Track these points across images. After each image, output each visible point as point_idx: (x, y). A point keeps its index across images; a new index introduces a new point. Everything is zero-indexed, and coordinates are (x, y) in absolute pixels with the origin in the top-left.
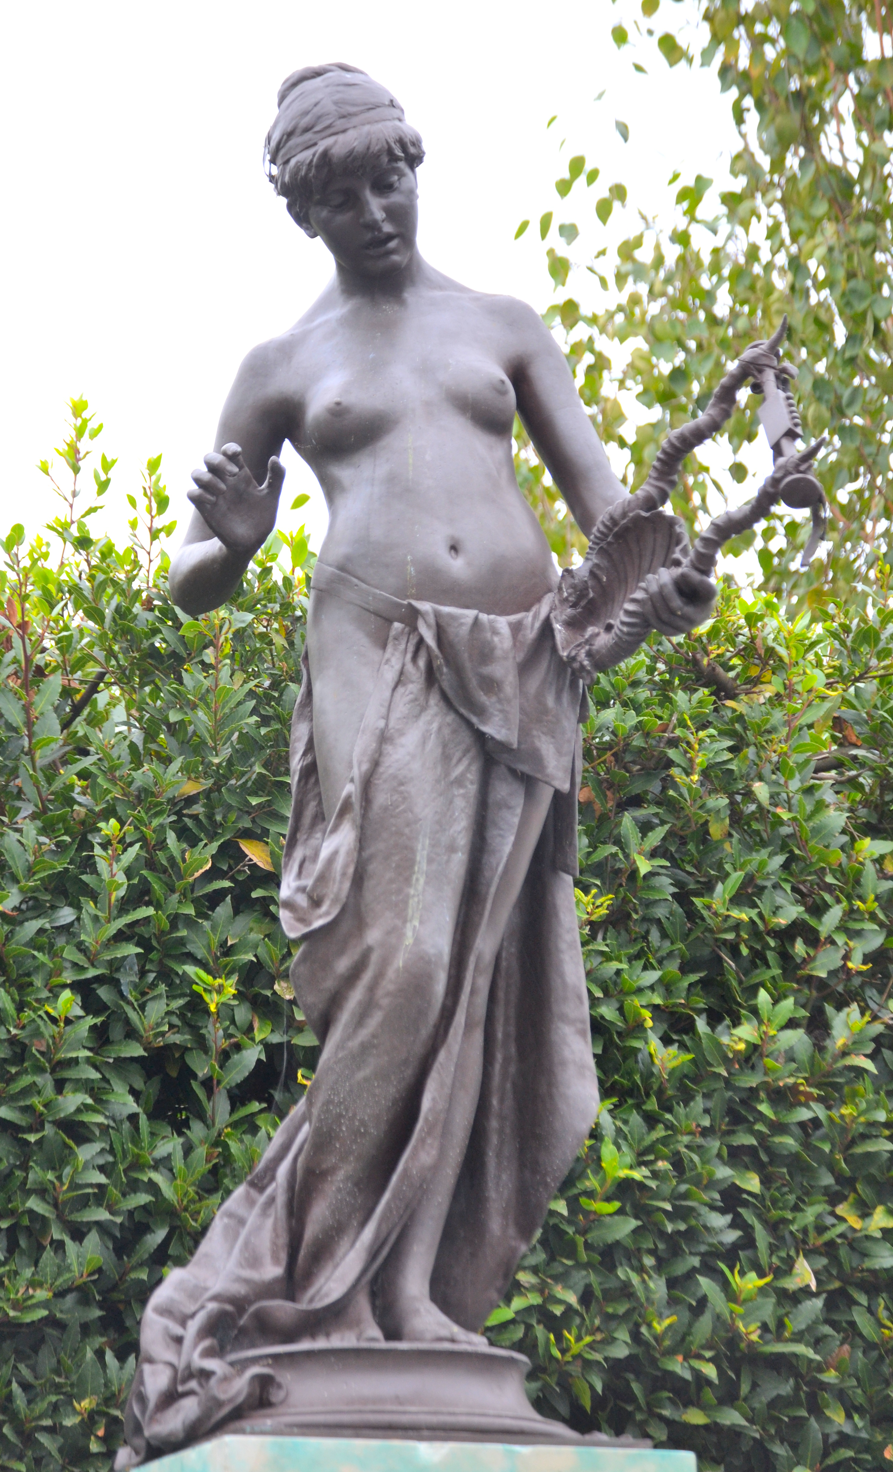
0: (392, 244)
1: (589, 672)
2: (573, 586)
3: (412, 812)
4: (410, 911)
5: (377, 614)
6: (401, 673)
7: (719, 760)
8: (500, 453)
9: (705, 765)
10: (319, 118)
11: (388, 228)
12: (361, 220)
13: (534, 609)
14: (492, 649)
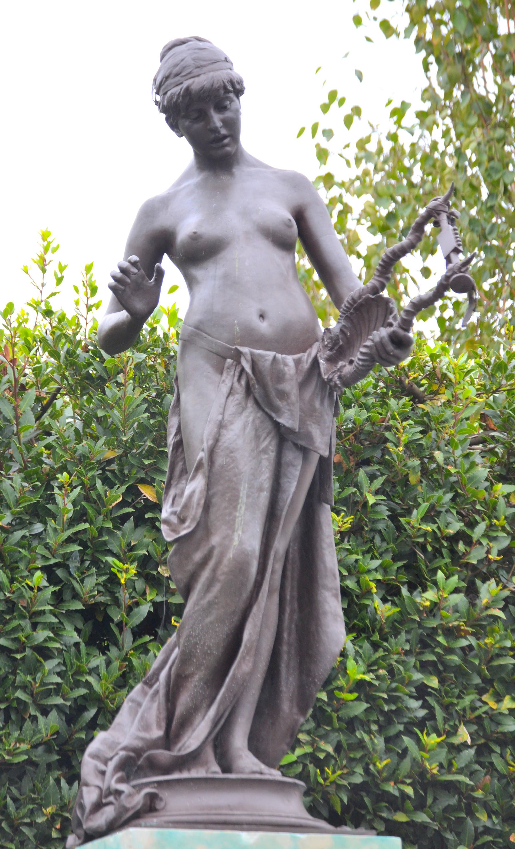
0: (226, 141)
1: (339, 388)
2: (331, 338)
3: (237, 468)
4: (236, 526)
5: (217, 354)
6: (232, 388)
7: (415, 438)
8: (288, 261)
9: (407, 441)
10: (184, 68)
11: (224, 132)
12: (208, 127)
13: (308, 351)
14: (284, 374)
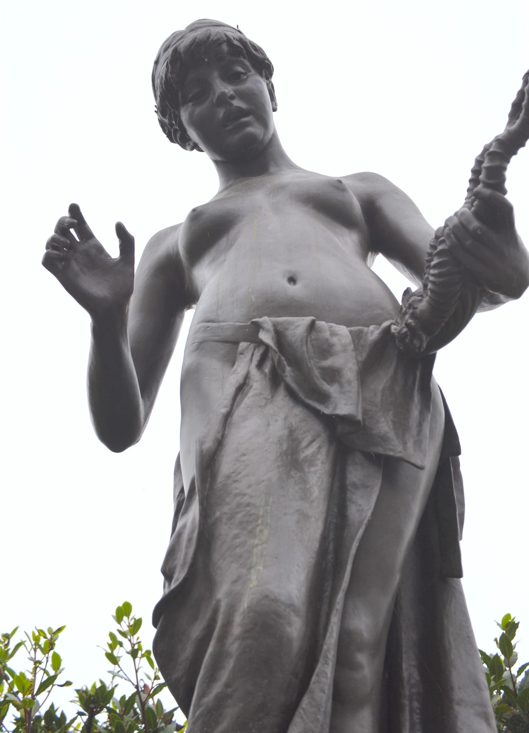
4: (254, 559)
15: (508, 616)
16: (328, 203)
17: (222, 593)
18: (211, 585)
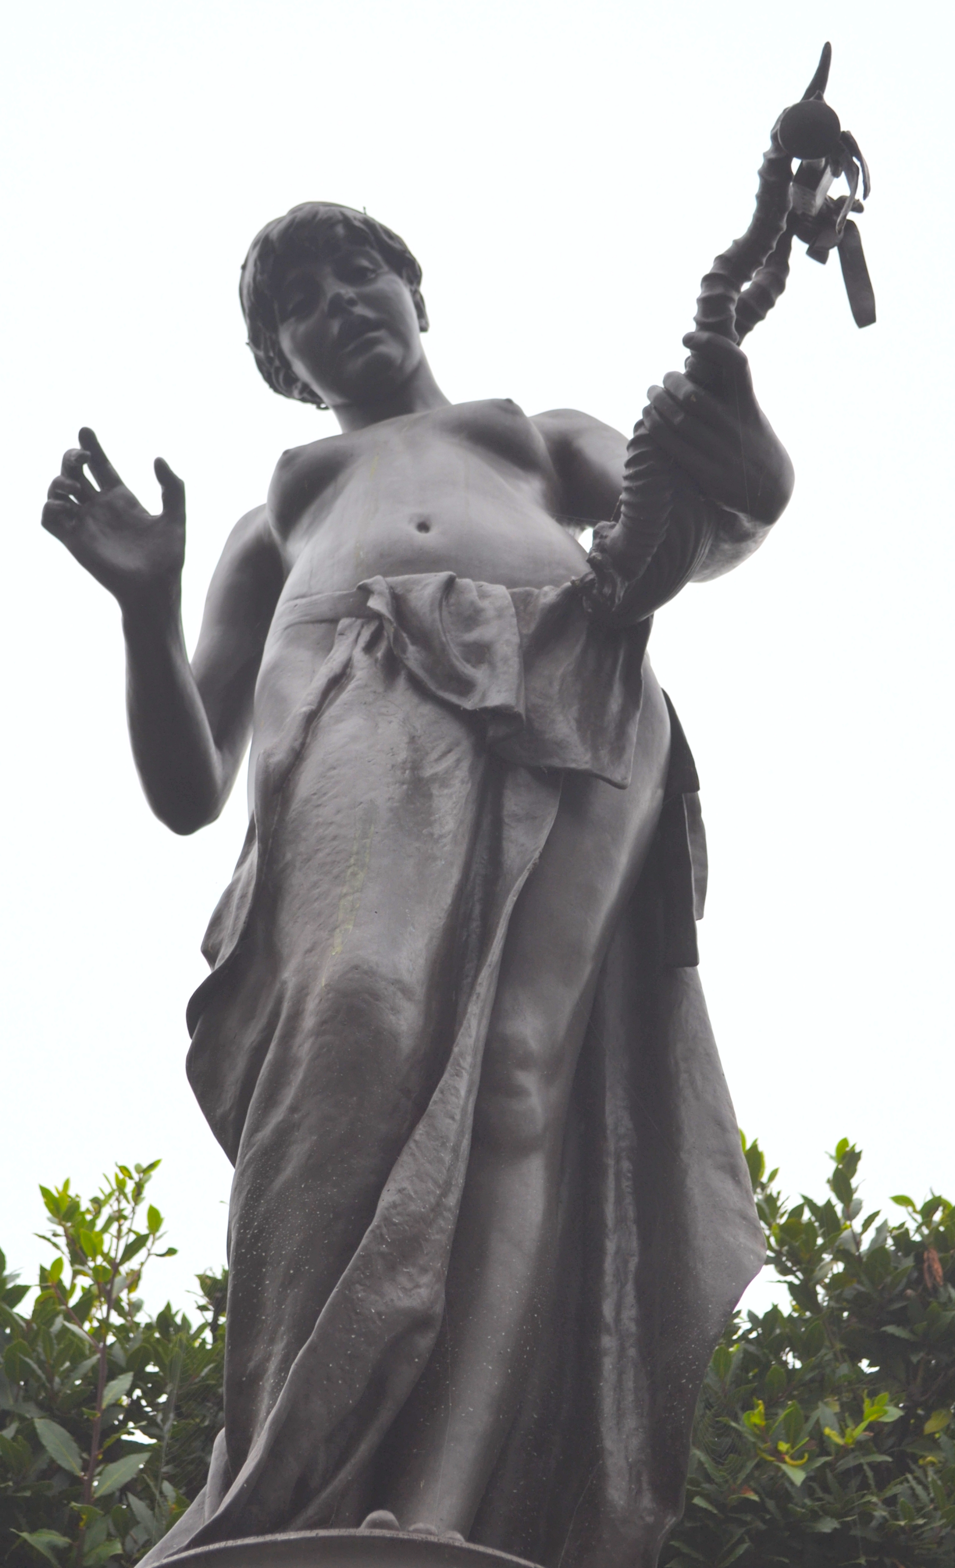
15: (844, 1142)
16: (496, 435)
17: (289, 975)
18: (274, 960)
